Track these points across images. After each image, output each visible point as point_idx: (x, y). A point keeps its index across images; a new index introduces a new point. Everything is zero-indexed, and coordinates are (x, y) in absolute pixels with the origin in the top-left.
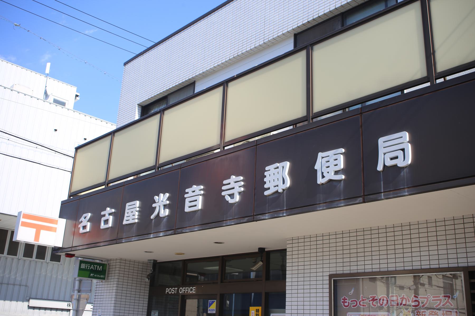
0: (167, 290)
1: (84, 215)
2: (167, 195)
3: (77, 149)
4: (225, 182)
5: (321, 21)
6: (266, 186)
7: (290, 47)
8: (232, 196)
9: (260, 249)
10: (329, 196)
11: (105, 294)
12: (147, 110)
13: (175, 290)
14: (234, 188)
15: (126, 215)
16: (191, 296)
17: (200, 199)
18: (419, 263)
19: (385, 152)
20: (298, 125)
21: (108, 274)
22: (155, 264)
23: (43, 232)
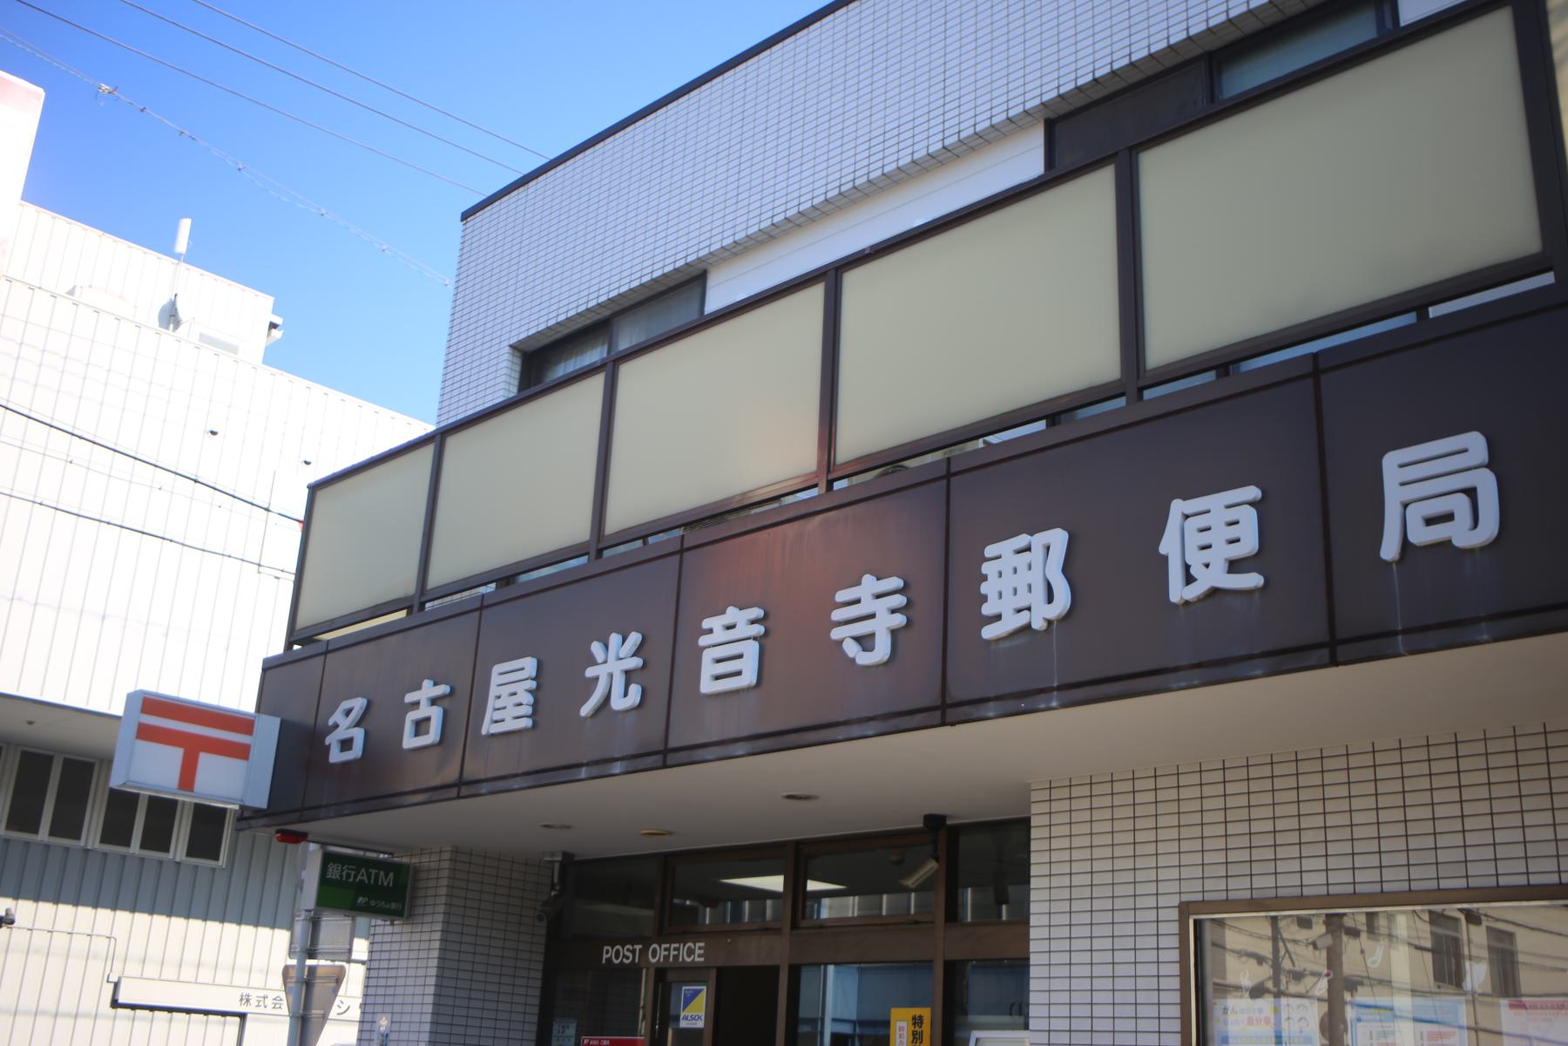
0: (608, 953)
1: (346, 705)
2: (635, 638)
3: (314, 489)
4: (841, 596)
5: (1137, 77)
6: (987, 610)
7: (1025, 159)
8: (865, 642)
9: (930, 819)
10: (1223, 645)
11: (403, 964)
12: (539, 365)
13: (633, 952)
14: (871, 615)
15: (491, 703)
16: (693, 973)
17: (751, 650)
18: (1374, 875)
19: (1406, 498)
20: (651, 540)
21: (414, 898)
22: (569, 862)
23: (206, 761)
